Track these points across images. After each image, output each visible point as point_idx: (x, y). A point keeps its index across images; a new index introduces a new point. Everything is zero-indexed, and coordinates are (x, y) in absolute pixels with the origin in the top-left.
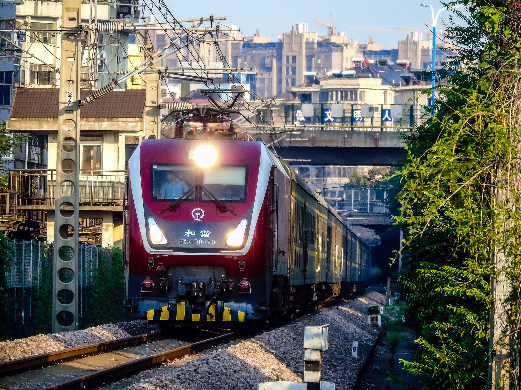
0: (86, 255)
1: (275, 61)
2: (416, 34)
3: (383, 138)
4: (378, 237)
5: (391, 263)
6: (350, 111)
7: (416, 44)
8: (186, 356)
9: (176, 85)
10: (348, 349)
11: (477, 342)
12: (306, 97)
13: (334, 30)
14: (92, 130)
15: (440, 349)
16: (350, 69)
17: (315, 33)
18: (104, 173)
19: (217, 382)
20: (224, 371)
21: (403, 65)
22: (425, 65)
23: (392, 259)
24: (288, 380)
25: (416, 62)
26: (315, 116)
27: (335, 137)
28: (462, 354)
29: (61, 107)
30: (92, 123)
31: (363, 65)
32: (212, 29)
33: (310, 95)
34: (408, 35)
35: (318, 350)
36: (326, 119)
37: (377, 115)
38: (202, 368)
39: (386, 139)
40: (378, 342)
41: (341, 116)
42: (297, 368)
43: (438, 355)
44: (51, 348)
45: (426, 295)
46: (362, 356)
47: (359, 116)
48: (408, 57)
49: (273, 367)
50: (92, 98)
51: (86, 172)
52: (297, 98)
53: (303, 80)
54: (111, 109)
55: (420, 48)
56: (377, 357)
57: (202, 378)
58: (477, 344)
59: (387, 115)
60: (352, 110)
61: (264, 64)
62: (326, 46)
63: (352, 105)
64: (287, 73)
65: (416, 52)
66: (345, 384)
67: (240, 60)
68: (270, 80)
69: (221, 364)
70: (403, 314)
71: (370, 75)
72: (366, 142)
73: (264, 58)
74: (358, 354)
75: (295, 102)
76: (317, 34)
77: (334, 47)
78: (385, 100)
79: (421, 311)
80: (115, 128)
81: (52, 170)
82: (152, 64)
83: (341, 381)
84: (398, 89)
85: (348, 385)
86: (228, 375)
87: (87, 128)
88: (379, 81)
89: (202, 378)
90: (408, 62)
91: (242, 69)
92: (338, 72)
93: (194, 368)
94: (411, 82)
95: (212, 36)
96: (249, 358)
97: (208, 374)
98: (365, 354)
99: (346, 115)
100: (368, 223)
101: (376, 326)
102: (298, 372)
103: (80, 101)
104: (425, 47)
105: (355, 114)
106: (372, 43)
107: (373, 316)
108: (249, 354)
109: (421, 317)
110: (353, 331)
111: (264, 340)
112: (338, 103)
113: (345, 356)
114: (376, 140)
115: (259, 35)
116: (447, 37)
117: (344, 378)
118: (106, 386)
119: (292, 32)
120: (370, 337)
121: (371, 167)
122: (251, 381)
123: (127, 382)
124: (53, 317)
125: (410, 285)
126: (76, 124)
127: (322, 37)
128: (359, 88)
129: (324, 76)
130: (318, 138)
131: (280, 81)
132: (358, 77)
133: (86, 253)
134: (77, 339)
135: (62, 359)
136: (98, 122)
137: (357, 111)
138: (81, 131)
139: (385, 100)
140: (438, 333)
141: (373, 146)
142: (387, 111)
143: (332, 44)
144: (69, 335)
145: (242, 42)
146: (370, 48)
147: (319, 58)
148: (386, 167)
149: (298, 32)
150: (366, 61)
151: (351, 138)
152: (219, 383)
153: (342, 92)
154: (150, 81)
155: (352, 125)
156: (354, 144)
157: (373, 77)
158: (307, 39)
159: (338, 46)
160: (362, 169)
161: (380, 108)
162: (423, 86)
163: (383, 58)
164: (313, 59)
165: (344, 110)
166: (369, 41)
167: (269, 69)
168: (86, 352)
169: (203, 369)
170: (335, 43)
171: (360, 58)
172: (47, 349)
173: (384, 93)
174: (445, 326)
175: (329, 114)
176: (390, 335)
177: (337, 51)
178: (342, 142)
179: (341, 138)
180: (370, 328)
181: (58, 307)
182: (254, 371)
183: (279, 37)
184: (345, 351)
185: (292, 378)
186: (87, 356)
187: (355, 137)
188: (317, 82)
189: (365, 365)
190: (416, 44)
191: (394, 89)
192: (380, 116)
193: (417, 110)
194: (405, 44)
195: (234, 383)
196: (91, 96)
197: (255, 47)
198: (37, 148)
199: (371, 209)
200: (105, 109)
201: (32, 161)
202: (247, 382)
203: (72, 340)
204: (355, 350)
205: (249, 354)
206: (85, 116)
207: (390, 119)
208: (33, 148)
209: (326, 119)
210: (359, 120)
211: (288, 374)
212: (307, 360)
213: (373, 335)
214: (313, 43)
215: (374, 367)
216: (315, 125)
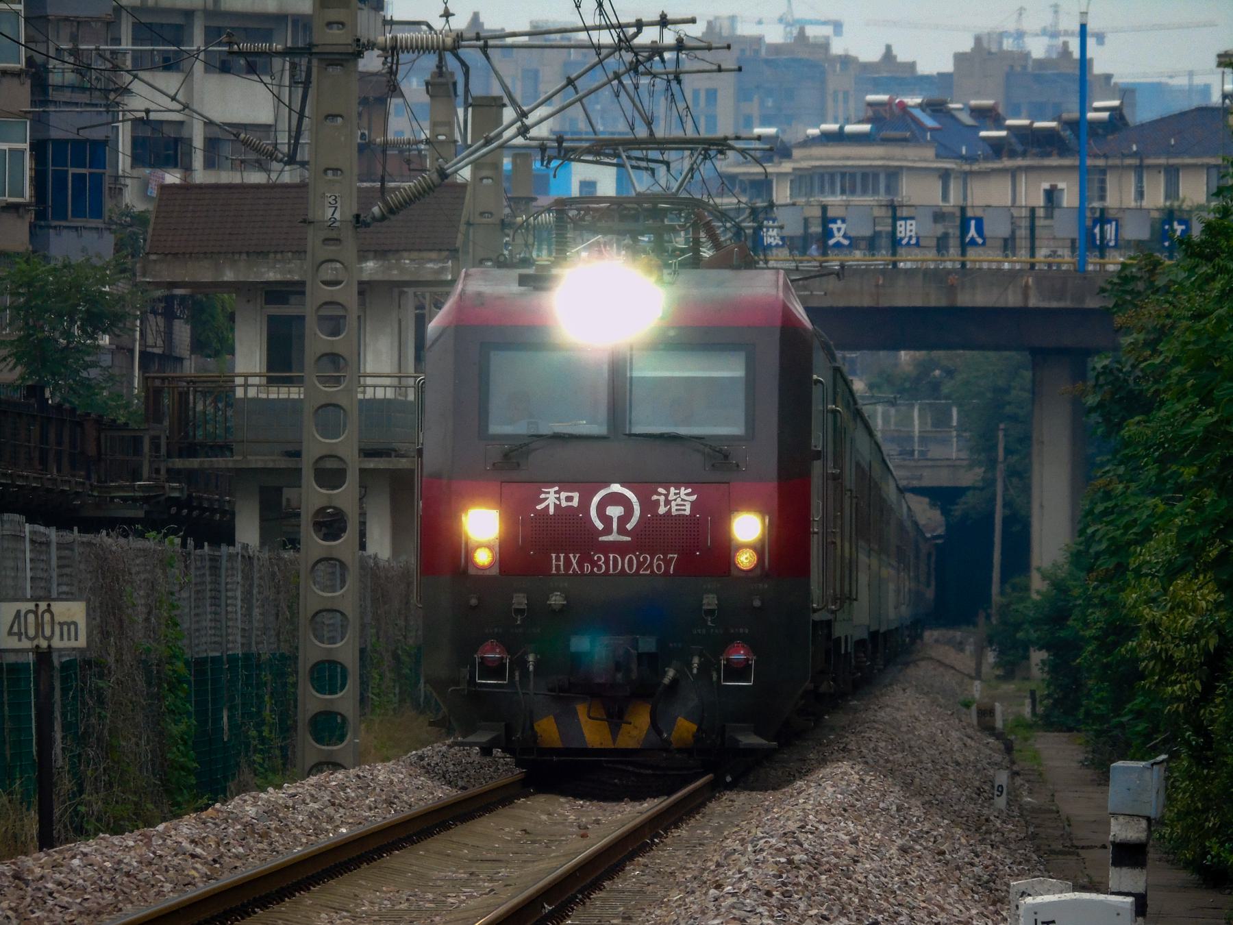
18: (369, 381)
35: (1143, 817)
36: (832, 242)
47: (908, 234)
59: (972, 232)
60: (895, 219)
80: (395, 275)
81: (246, 376)
105: (899, 229)
114: (952, 290)
124: (300, 724)
137: (903, 222)
141: (943, 303)
142: (973, 223)
155: (894, 254)
156: (901, 302)
175: (839, 229)
198: (159, 318)
201: (149, 350)
207: (980, 241)
208: (151, 317)
209: (832, 242)
210: (908, 244)
212: (1118, 841)
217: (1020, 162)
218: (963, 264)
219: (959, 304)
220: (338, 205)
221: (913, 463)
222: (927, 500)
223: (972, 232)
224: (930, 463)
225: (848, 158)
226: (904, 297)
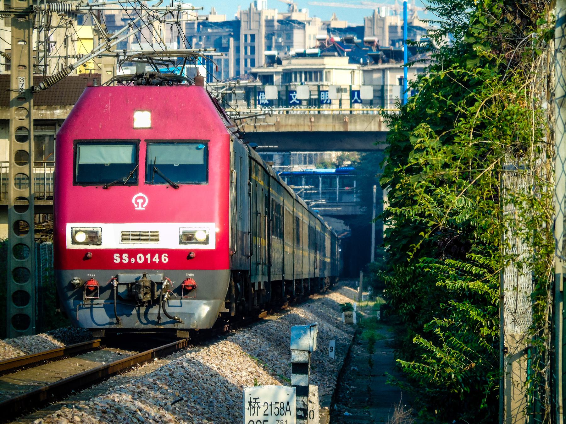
0: (41, 253)
1: (232, 39)
2: (383, 9)
3: (353, 121)
4: (348, 228)
5: (409, 258)
6: (317, 93)
7: (383, 20)
8: (156, 359)
9: (127, 69)
10: (324, 349)
11: (481, 339)
12: (267, 79)
13: (295, 6)
14: (44, 118)
15: (441, 347)
16: (314, 48)
17: (274, 9)
19: (194, 387)
20: (200, 375)
21: (371, 43)
22: (393, 43)
23: (410, 254)
24: (267, 383)
25: (384, 39)
26: (280, 98)
27: (301, 121)
28: (465, 353)
29: (14, 95)
30: (43, 112)
31: (328, 44)
32: (173, 8)
33: (272, 76)
34: (374, 11)
36: (291, 102)
37: (346, 96)
38: (177, 372)
39: (356, 122)
40: (355, 341)
41: (307, 97)
42: (275, 371)
43: (439, 355)
44: (10, 354)
45: (409, 290)
46: (339, 356)
47: (326, 98)
48: (375, 33)
49: (249, 370)
50: (46, 84)
51: (38, 165)
52: (258, 79)
53: (263, 61)
54: (64, 96)
55: (387, 24)
56: (354, 357)
57: (179, 382)
58: (482, 342)
59: (356, 97)
60: (319, 92)
61: (221, 44)
62: (288, 24)
63: (319, 87)
64: (246, 53)
65: (383, 28)
66: (325, 387)
67: (194, 40)
68: (227, 61)
69: (197, 368)
70: (377, 310)
71: (336, 54)
72: (334, 126)
73: (220, 38)
74: (335, 355)
75: (257, 84)
76: (277, 11)
77: (296, 25)
78: (352, 81)
79: (404, 306)
82: (110, 47)
83: (320, 383)
84: (366, 68)
85: (328, 387)
86: (205, 379)
87: (39, 117)
88: (346, 59)
89: (179, 382)
90: (376, 39)
91: (205, 50)
92: (301, 50)
93: (169, 372)
94: (380, 60)
95: (173, 15)
96: (224, 360)
97: (183, 378)
98: (342, 354)
99: (312, 97)
100: (336, 213)
101: (351, 324)
102: (276, 375)
103: (33, 87)
104: (393, 24)
106: (336, 19)
107: (347, 313)
108: (224, 357)
109: (403, 313)
110: (328, 329)
111: (238, 342)
112: (302, 84)
113: (322, 356)
114: (345, 124)
115: (215, 14)
116: (429, 9)
117: (324, 381)
118: (76, 394)
119: (250, 9)
120: (346, 336)
121: (339, 153)
122: (229, 385)
123: (98, 389)
125: (391, 279)
126: (29, 112)
127: (282, 14)
128: (324, 68)
129: (286, 56)
130: (283, 122)
131: (238, 61)
132: (322, 56)
133: (41, 250)
134: (37, 344)
135: (24, 366)
136: (50, 110)
138: (35, 120)
139: (352, 81)
140: (438, 331)
141: (342, 129)
142: (356, 93)
143: (294, 21)
144: (28, 339)
145: (196, 22)
146: (334, 25)
147: (279, 36)
148: (356, 153)
149: (257, 9)
150: (332, 39)
151: (318, 122)
152: (196, 388)
153: (306, 73)
154: (105, 66)
156: (322, 129)
157: (340, 55)
158: (267, 17)
159: (300, 23)
160: (330, 155)
161: (348, 89)
162: (393, 64)
163: (349, 36)
164: (273, 38)
165: (310, 92)
166: (333, 17)
167: (226, 49)
168: (48, 357)
169: (178, 373)
170: (297, 21)
171: (324, 35)
172: (5, 355)
173: (351, 73)
174: (446, 322)
175: (294, 96)
176: (366, 334)
177: (299, 28)
178: (309, 126)
179: (307, 122)
180: (344, 326)
181: (13, 309)
182: (230, 375)
183: (236, 15)
184: (322, 351)
185: (270, 381)
186: (49, 362)
187: (322, 120)
188: (279, 62)
189: (343, 366)
190: (383, 20)
191: (361, 68)
192: (349, 98)
193: (387, 90)
194: (371, 20)
195: (212, 388)
196: (45, 82)
197: (211, 26)
199: (340, 199)
200: (57, 96)
202: (225, 387)
203: (32, 345)
204: (332, 350)
205: (224, 357)
206: (38, 104)
211: (266, 377)
212: (295, 362)
213: (348, 333)
214: (272, 21)
215: (352, 368)
216: (279, 109)
217: (386, 66)
218: (351, 112)
219: (349, 130)
220: (24, 82)
221: (336, 204)
222: (343, 221)
223: (356, 97)
224: (343, 204)
225: (308, 65)
226: (324, 126)
